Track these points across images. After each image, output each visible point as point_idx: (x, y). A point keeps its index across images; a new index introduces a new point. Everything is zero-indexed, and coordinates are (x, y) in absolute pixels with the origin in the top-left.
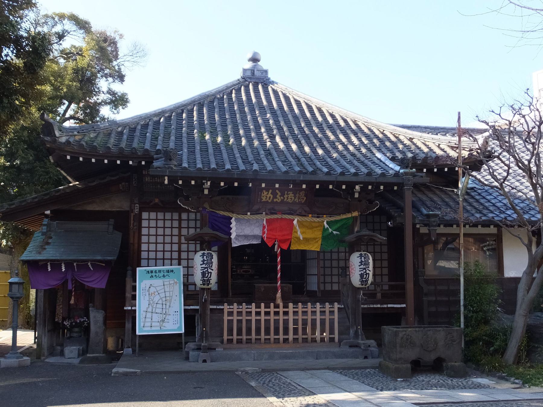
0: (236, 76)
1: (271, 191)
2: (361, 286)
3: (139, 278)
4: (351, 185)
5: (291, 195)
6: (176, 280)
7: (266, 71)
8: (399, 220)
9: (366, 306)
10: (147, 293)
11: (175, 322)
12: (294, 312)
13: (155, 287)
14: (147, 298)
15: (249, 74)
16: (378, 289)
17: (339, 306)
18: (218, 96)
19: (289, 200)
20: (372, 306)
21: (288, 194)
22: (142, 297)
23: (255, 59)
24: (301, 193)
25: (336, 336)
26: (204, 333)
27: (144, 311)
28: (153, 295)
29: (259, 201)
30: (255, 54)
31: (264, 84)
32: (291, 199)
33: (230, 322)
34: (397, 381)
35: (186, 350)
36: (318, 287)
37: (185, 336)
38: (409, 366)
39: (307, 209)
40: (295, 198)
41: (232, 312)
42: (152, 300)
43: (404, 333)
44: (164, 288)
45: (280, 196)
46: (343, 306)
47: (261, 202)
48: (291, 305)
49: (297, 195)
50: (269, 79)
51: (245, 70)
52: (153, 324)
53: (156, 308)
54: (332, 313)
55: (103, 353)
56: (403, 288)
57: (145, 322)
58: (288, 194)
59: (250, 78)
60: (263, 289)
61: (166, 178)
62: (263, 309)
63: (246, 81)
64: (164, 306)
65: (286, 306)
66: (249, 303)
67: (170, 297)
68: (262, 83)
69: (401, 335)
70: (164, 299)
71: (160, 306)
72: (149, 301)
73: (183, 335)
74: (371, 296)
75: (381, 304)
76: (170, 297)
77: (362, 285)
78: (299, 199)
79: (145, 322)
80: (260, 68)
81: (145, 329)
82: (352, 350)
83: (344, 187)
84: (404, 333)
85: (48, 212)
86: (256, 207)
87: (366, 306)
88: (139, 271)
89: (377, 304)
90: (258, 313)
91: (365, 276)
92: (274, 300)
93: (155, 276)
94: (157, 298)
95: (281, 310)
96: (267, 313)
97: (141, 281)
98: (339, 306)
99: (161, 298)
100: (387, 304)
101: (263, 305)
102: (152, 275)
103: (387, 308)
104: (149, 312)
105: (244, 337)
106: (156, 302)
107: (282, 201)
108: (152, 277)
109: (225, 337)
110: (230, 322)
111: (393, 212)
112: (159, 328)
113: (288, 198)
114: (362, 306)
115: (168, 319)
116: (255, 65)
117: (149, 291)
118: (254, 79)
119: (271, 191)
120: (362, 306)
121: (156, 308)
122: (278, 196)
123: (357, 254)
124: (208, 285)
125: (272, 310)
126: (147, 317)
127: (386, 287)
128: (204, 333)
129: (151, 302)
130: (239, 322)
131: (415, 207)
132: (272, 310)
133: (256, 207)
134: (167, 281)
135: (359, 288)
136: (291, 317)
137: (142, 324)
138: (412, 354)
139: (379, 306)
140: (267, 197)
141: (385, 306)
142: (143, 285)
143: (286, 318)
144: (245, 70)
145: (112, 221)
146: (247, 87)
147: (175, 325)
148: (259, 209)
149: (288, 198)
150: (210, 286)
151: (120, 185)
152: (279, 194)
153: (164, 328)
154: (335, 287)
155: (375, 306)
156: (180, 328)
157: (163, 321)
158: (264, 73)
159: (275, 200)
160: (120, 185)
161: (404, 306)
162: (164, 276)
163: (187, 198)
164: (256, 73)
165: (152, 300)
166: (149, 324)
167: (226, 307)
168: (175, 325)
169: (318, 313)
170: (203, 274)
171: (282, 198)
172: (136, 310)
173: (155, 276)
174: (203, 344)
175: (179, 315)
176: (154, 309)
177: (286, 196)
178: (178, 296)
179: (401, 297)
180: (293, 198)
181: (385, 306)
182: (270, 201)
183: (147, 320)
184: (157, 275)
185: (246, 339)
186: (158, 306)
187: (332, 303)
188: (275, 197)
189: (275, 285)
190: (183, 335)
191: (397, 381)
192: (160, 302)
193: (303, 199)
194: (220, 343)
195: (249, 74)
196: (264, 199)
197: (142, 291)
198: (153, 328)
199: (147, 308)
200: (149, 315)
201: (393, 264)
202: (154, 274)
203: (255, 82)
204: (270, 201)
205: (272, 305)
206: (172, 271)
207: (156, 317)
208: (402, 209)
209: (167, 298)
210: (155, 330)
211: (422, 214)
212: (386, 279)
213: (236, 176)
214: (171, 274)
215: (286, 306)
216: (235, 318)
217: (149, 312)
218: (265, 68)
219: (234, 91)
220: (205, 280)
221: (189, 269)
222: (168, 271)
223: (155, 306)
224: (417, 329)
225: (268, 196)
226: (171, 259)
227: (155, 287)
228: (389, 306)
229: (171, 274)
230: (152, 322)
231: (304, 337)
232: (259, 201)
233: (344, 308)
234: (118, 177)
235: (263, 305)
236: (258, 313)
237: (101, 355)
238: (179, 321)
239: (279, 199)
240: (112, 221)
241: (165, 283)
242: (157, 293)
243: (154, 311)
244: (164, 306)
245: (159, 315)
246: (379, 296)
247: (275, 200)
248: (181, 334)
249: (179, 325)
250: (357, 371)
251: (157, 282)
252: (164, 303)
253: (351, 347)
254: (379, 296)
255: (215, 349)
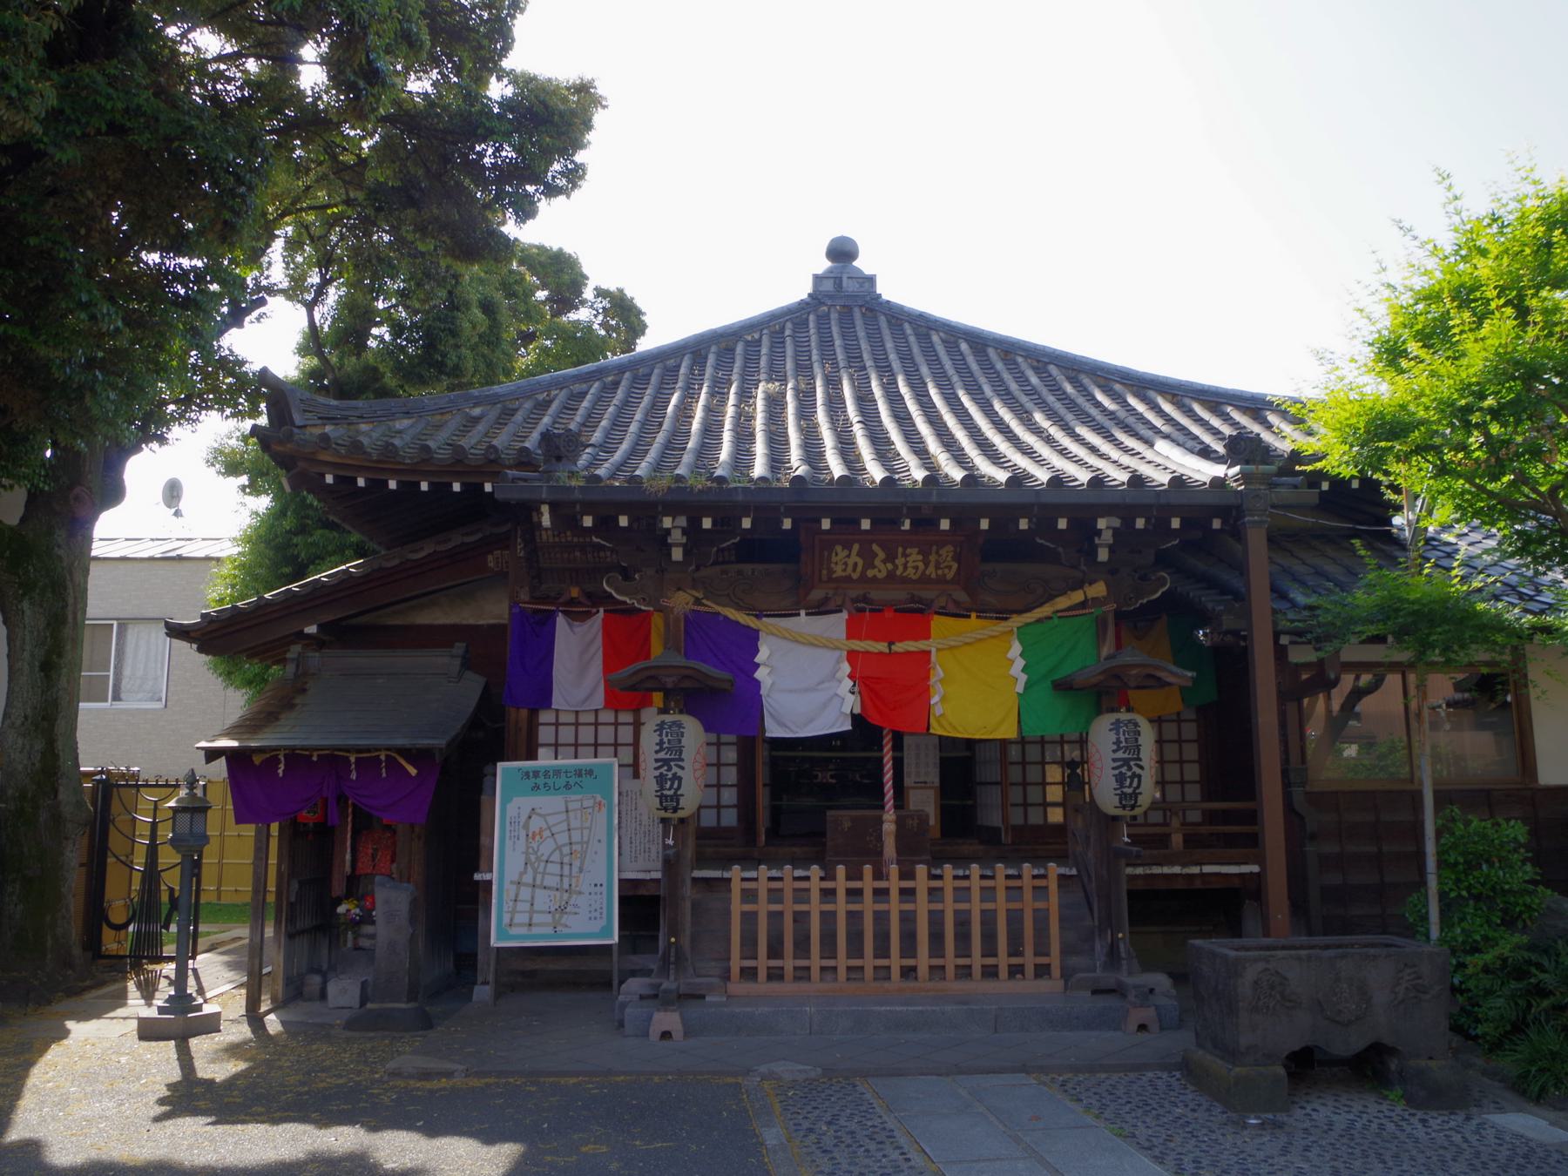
0: (797, 290)
1: (856, 547)
2: (1119, 812)
4: (1084, 528)
5: (915, 556)
6: (599, 798)
8: (1228, 622)
9: (1139, 871)
10: (523, 833)
12: (931, 891)
15: (828, 286)
16: (1175, 823)
17: (1063, 870)
19: (910, 571)
20: (1156, 870)
21: (905, 555)
22: (508, 843)
24: (943, 552)
25: (1055, 960)
29: (824, 578)
32: (916, 568)
33: (749, 919)
34: (1245, 1126)
35: (621, 998)
36: (1005, 819)
37: (621, 953)
38: (1281, 1071)
39: (962, 596)
40: (927, 565)
41: (759, 889)
43: (1261, 966)
44: (568, 819)
45: (884, 562)
46: (1074, 872)
47: (830, 579)
48: (921, 870)
49: (933, 558)
51: (818, 279)
52: (537, 918)
53: (544, 873)
54: (1040, 892)
55: (409, 1001)
56: (1252, 817)
57: (513, 912)
58: (905, 555)
59: (831, 297)
60: (847, 825)
61: (545, 509)
62: (841, 883)
64: (566, 868)
65: (907, 874)
66: (805, 862)
67: (581, 843)
69: (1251, 974)
70: (566, 850)
72: (527, 853)
73: (615, 949)
74: (1152, 842)
75: (1184, 865)
77: (1124, 807)
78: (937, 567)
79: (513, 912)
81: (514, 931)
82: (1102, 1002)
83: (1062, 524)
84: (1261, 966)
85: (312, 629)
86: (817, 594)
87: (1139, 871)
89: (1172, 864)
90: (829, 894)
92: (874, 854)
94: (546, 848)
95: (894, 884)
96: (854, 894)
98: (1063, 870)
99: (559, 848)
100: (1201, 864)
101: (841, 870)
102: (540, 782)
103: (1202, 875)
104: (526, 885)
105: (789, 963)
107: (891, 576)
108: (536, 787)
109: (736, 963)
110: (749, 919)
111: (1209, 600)
112: (549, 930)
113: (905, 568)
114: (1129, 870)
115: (575, 906)
117: (526, 826)
119: (856, 547)
120: (1129, 870)
121: (544, 873)
122: (877, 562)
123: (1106, 720)
125: (868, 883)
127: (1194, 816)
129: (533, 858)
130: (775, 917)
131: (1279, 593)
132: (868, 883)
133: (817, 594)
135: (1115, 818)
136: (922, 906)
137: (506, 920)
138: (1291, 1034)
139: (1177, 870)
140: (846, 564)
141: (1195, 870)
142: (512, 809)
143: (908, 907)
145: (459, 648)
146: (823, 321)
147: (594, 922)
148: (826, 600)
149: (905, 568)
151: (490, 558)
152: (881, 555)
153: (566, 931)
154: (1056, 816)
155: (1166, 870)
156: (606, 931)
157: (562, 910)
159: (870, 573)
160: (490, 558)
161: (1255, 869)
162: (568, 786)
163: (627, 574)
166: (524, 918)
167: (736, 873)
168: (594, 922)
169: (1001, 895)
171: (890, 566)
172: (490, 882)
176: (539, 877)
177: (900, 561)
179: (1250, 844)
180: (921, 565)
181: (1195, 870)
182: (855, 576)
183: (522, 906)
184: (550, 782)
185: (795, 968)
187: (1038, 859)
188: (869, 564)
189: (877, 812)
190: (615, 949)
191: (1245, 1126)
192: (556, 857)
193: (950, 567)
194: (715, 980)
195: (828, 286)
196: (839, 571)
197: (508, 828)
198: (535, 930)
199: (521, 874)
200: (525, 893)
201: (1222, 744)
202: (540, 781)
204: (855, 576)
205: (868, 869)
206: (590, 772)
207: (543, 900)
208: (1240, 598)
211: (1294, 605)
212: (1194, 793)
213: (740, 498)
214: (586, 780)
215: (907, 874)
216: (763, 908)
217: (526, 885)
218: (867, 271)
219: (789, 325)
222: (579, 773)
224: (1303, 953)
225: (851, 562)
226: (616, 745)
228: (1207, 869)
230: (532, 912)
231: (961, 961)
232: (824, 578)
233: (1079, 876)
234: (479, 535)
235: (841, 870)
236: (829, 894)
237: (403, 1006)
239: (880, 570)
240: (459, 648)
241: (571, 806)
242: (547, 833)
243: (538, 882)
244: (566, 868)
245: (552, 893)
246: (1177, 840)
247: (870, 573)
248: (609, 947)
249: (604, 922)
250: (1115, 1077)
251: (550, 803)
252: (566, 860)
253: (1095, 992)
254: (1177, 840)
255: (703, 997)
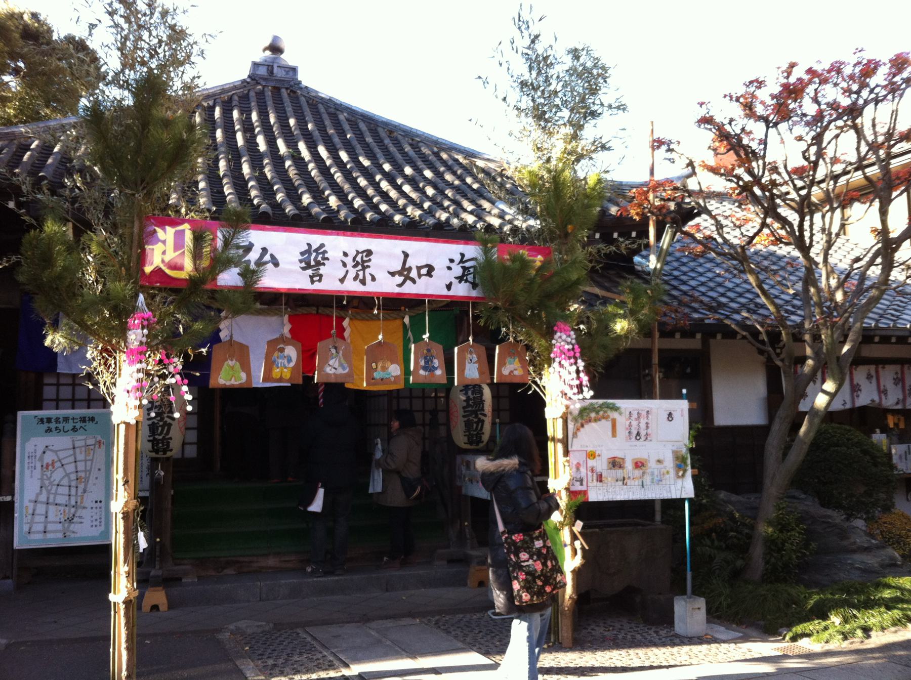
3: (22, 432)
7: (294, 70)
10: (39, 465)
11: (95, 523)
13: (56, 452)
14: (38, 472)
18: (205, 104)
22: (27, 472)
23: (275, 48)
26: (158, 547)
27: (30, 501)
28: (50, 468)
30: (276, 38)
31: (291, 91)
42: (49, 479)
44: (74, 454)
50: (300, 82)
51: (255, 65)
52: (50, 527)
53: (56, 494)
59: (265, 79)
63: (258, 83)
64: (73, 491)
67: (85, 471)
68: (287, 89)
70: (73, 477)
71: (65, 490)
72: (42, 479)
76: (85, 471)
80: (283, 63)
88: (23, 417)
91: (475, 425)
93: (57, 428)
94: (58, 475)
97: (25, 440)
99: (67, 475)
102: (50, 426)
104: (41, 502)
106: (56, 482)
108: (49, 430)
115: (80, 517)
116: (275, 58)
117: (41, 459)
118: (272, 81)
124: (165, 452)
126: (37, 512)
128: (158, 547)
129: (47, 482)
134: (80, 439)
137: (26, 528)
142: (30, 447)
144: (255, 65)
150: (169, 454)
153: (72, 535)
158: (291, 73)
162: (74, 429)
164: (276, 70)
165: (49, 479)
166: (40, 527)
170: (468, 424)
173: (57, 428)
174: (153, 573)
175: (103, 509)
176: (52, 497)
178: (103, 470)
183: (37, 519)
184: (60, 426)
186: (61, 490)
192: (65, 482)
197: (27, 460)
198: (49, 536)
199: (38, 495)
200: (41, 509)
202: (53, 425)
203: (274, 87)
206: (92, 419)
209: (80, 474)
210: (54, 539)
217: (41, 502)
218: (291, 63)
220: (158, 440)
221: (55, 403)
222: (83, 420)
223: (53, 491)
227: (56, 452)
229: (89, 425)
230: (46, 523)
238: (103, 520)
241: (77, 444)
242: (58, 464)
243: (51, 500)
244: (73, 491)
245: (61, 508)
249: (103, 528)
251: (60, 442)
252: (73, 484)
255: (180, 579)
